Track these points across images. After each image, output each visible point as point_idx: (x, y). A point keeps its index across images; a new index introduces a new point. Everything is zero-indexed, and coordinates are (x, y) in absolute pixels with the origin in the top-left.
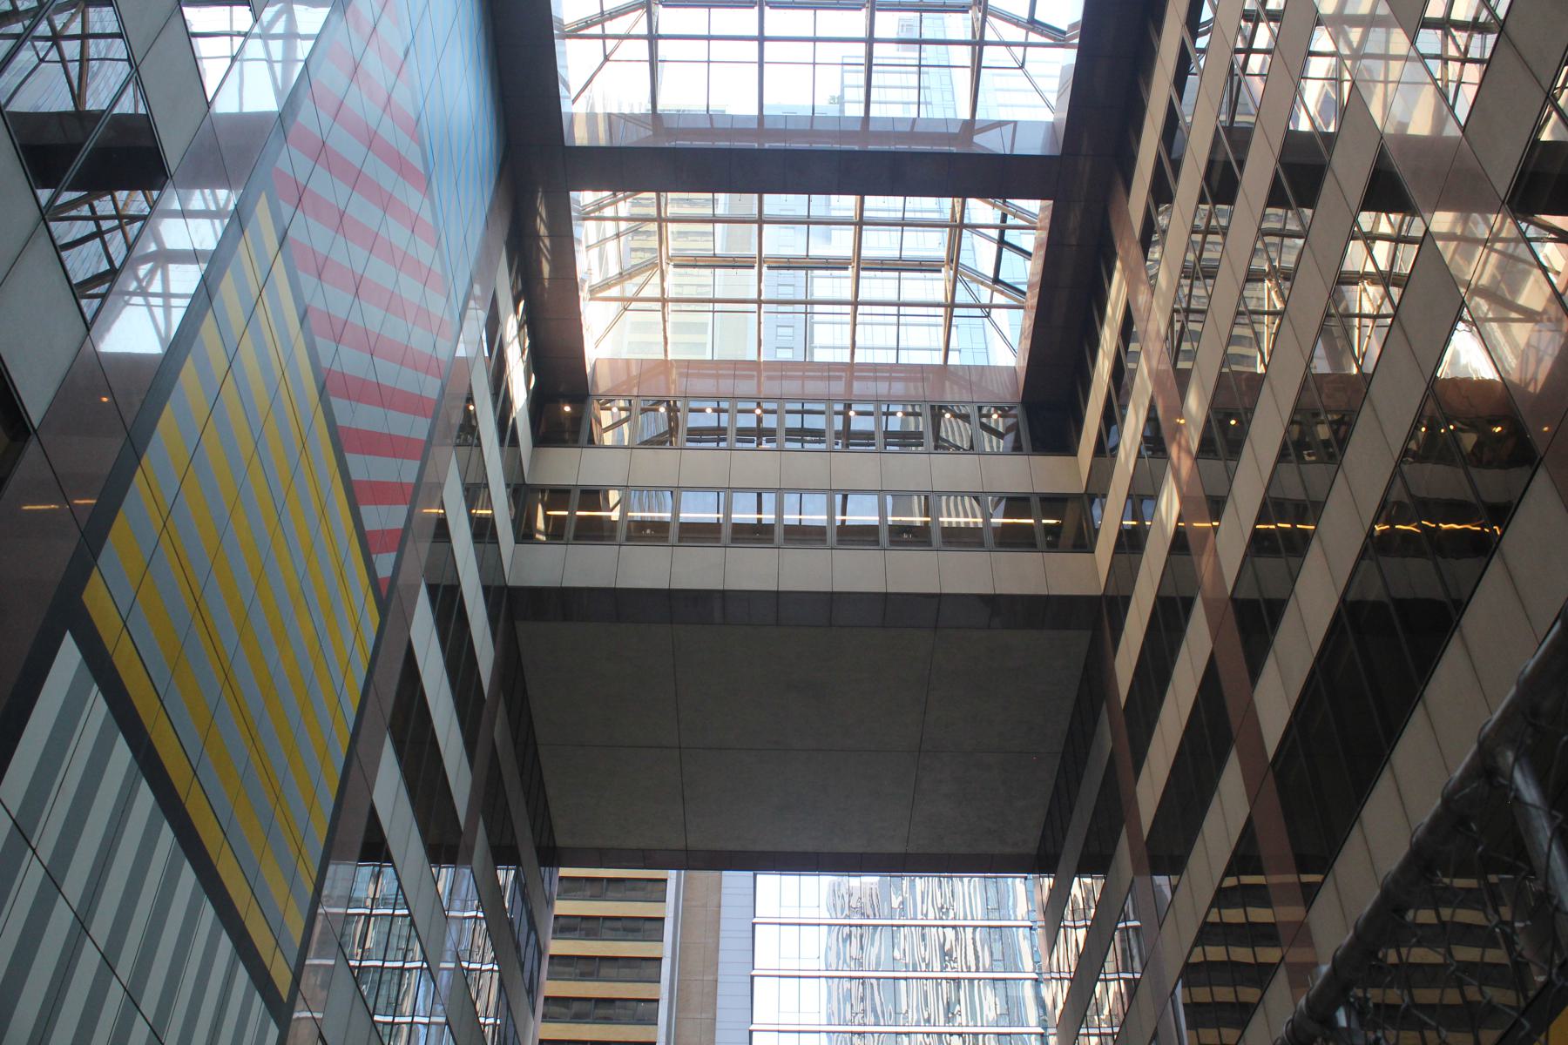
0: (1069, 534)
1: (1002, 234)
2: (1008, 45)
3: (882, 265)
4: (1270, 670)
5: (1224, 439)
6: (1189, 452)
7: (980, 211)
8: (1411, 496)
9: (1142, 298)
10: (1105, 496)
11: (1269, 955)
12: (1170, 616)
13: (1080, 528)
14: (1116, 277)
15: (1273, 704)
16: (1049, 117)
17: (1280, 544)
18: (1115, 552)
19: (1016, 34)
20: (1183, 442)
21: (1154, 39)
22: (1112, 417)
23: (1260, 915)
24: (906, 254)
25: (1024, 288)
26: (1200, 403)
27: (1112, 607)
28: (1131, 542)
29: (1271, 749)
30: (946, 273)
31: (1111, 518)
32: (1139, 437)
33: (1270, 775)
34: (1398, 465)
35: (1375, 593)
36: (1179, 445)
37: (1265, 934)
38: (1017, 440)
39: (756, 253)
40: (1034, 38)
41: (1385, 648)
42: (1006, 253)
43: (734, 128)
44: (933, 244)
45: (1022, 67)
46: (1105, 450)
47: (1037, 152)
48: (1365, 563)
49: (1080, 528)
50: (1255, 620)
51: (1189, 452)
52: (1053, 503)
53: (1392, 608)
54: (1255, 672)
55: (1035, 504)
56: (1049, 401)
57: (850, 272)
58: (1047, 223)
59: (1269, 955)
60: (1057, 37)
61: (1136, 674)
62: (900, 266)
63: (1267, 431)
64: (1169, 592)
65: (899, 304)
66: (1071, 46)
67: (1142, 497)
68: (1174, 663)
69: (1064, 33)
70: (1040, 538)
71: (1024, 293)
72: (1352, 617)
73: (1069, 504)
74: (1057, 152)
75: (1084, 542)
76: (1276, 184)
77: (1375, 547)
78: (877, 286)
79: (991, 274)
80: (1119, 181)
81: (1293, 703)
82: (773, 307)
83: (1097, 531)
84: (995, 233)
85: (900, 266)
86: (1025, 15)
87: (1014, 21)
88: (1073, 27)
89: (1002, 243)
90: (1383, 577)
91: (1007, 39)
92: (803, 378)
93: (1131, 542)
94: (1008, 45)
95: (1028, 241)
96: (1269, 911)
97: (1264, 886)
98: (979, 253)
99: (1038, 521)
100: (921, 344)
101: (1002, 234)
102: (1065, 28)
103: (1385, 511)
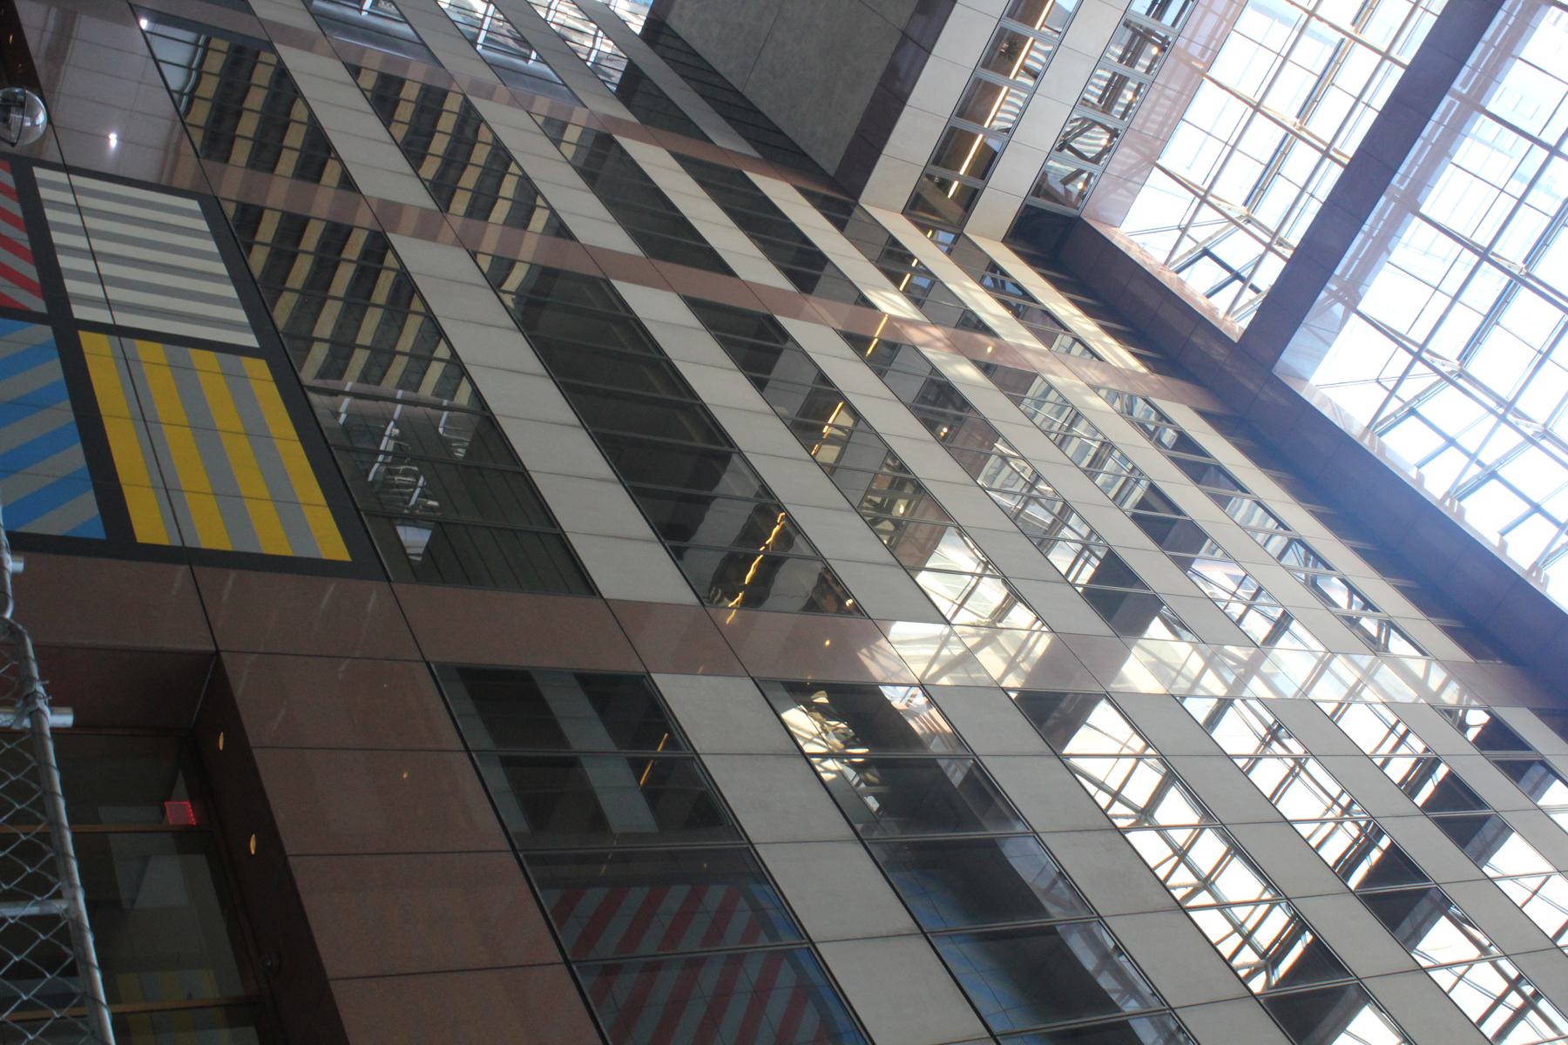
0: (931, 196)
1: (1242, 279)
2: (1400, 380)
3: (1281, 152)
4: (687, 317)
5: (938, 403)
6: (926, 345)
7: (1270, 273)
8: (714, 498)
9: (1094, 374)
10: (949, 253)
11: (460, 203)
12: (805, 267)
13: (934, 212)
14: (1133, 363)
15: (660, 309)
16: (1315, 380)
17: (812, 409)
18: (891, 236)
19: (1408, 391)
20: (940, 345)
21: (1356, 544)
22: (1021, 305)
23: (501, 211)
24: (1279, 180)
25: (1183, 275)
26: (962, 377)
27: (840, 205)
28: (894, 260)
29: (622, 287)
30: (1238, 210)
31: (924, 248)
32: (973, 308)
33: (600, 275)
34: (823, 559)
35: (729, 483)
36: (939, 340)
37: (480, 208)
38: (1050, 195)
39: (1365, 37)
40: (1394, 405)
41: (672, 460)
42: (1226, 275)
43: (1490, 77)
44: (1269, 212)
45: (1378, 381)
46: (996, 280)
47: (1286, 357)
48: (756, 485)
49: (934, 212)
50: (755, 343)
51: (926, 345)
52: (969, 198)
53: (705, 493)
54: (694, 304)
55: (975, 183)
56: (1061, 239)
57: (1291, 120)
58: (1366, 443)
59: (460, 203)
60: (1378, 425)
61: (766, 198)
62: (1272, 169)
63: (927, 458)
64: (828, 268)
65: (1233, 148)
66: (1363, 435)
67: (925, 292)
68: (751, 237)
69: (1460, 499)
70: (940, 172)
71: (1178, 272)
72: (714, 450)
73: (960, 210)
74: (1278, 370)
75: (918, 208)
76: (1131, 578)
77: (767, 505)
78: (1264, 138)
79: (1213, 251)
80: (1368, 547)
81: (646, 324)
82: (1302, 22)
83: (924, 228)
84: (1245, 274)
85: (1272, 169)
86: (1501, 473)
87: (1504, 459)
88: (1461, 512)
89: (1236, 276)
90: (738, 499)
91: (1406, 382)
92: (1222, 18)
93: (894, 260)
94: (1400, 380)
95: (1221, 302)
96: (501, 221)
97: (525, 226)
98: (1239, 250)
99: (959, 178)
100: (1187, 151)
101: (1242, 279)
102: (1463, 503)
103: (792, 531)
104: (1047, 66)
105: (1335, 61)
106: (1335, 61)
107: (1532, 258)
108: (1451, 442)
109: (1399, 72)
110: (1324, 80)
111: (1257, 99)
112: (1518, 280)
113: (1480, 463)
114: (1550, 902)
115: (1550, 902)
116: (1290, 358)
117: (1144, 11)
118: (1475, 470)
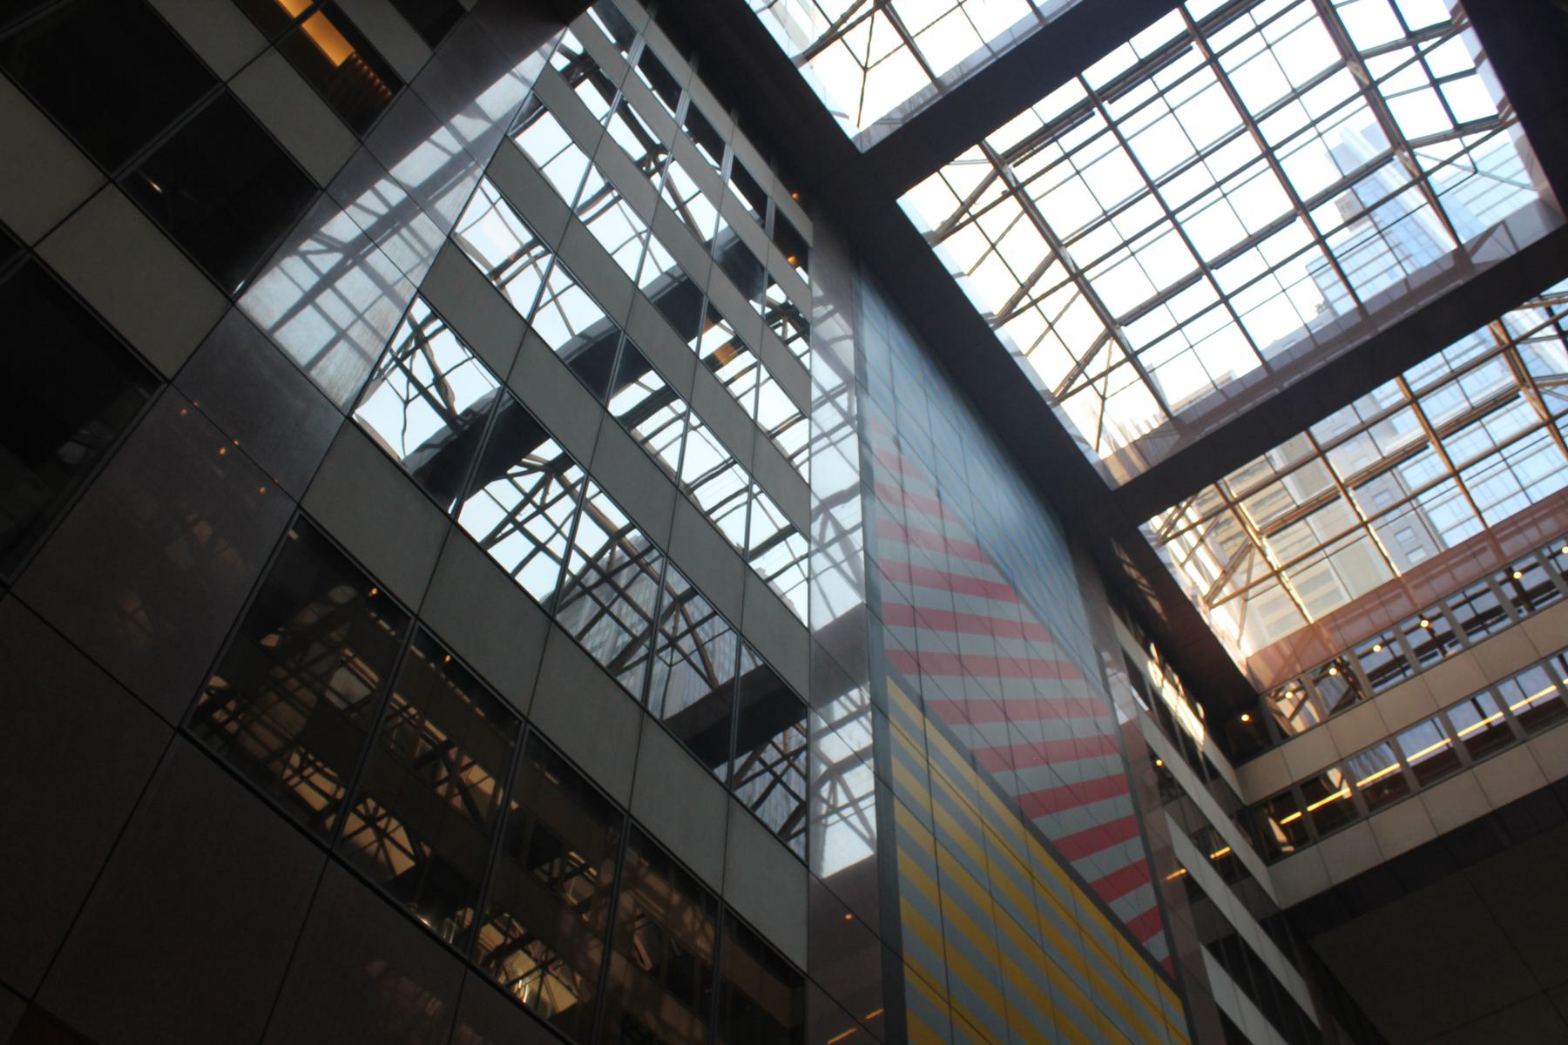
2: (1449, 161)
16: (1531, 196)
44: (1496, 376)
45: (1476, 171)
78: (1464, 446)
92: (1449, 569)
94: (1449, 161)
104: (1551, 656)
105: (1458, 425)
106: (1458, 425)
107: (1287, 221)
108: (1435, 83)
109: (1410, 375)
110: (1476, 415)
111: (1544, 431)
112: (1303, 209)
113: (1416, 49)
114: (1073, 299)
115: (1073, 299)
116: (1535, 230)
117: (1368, 671)
118: (1423, 46)
